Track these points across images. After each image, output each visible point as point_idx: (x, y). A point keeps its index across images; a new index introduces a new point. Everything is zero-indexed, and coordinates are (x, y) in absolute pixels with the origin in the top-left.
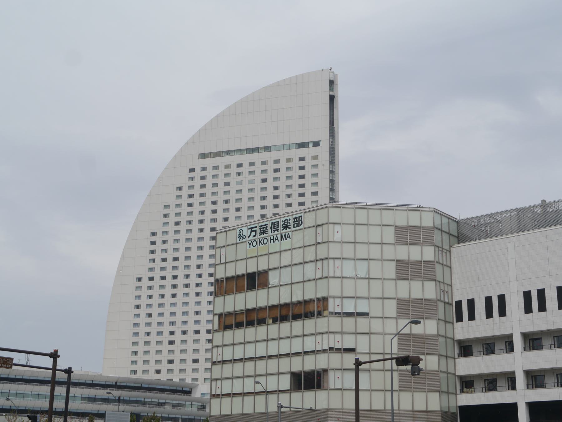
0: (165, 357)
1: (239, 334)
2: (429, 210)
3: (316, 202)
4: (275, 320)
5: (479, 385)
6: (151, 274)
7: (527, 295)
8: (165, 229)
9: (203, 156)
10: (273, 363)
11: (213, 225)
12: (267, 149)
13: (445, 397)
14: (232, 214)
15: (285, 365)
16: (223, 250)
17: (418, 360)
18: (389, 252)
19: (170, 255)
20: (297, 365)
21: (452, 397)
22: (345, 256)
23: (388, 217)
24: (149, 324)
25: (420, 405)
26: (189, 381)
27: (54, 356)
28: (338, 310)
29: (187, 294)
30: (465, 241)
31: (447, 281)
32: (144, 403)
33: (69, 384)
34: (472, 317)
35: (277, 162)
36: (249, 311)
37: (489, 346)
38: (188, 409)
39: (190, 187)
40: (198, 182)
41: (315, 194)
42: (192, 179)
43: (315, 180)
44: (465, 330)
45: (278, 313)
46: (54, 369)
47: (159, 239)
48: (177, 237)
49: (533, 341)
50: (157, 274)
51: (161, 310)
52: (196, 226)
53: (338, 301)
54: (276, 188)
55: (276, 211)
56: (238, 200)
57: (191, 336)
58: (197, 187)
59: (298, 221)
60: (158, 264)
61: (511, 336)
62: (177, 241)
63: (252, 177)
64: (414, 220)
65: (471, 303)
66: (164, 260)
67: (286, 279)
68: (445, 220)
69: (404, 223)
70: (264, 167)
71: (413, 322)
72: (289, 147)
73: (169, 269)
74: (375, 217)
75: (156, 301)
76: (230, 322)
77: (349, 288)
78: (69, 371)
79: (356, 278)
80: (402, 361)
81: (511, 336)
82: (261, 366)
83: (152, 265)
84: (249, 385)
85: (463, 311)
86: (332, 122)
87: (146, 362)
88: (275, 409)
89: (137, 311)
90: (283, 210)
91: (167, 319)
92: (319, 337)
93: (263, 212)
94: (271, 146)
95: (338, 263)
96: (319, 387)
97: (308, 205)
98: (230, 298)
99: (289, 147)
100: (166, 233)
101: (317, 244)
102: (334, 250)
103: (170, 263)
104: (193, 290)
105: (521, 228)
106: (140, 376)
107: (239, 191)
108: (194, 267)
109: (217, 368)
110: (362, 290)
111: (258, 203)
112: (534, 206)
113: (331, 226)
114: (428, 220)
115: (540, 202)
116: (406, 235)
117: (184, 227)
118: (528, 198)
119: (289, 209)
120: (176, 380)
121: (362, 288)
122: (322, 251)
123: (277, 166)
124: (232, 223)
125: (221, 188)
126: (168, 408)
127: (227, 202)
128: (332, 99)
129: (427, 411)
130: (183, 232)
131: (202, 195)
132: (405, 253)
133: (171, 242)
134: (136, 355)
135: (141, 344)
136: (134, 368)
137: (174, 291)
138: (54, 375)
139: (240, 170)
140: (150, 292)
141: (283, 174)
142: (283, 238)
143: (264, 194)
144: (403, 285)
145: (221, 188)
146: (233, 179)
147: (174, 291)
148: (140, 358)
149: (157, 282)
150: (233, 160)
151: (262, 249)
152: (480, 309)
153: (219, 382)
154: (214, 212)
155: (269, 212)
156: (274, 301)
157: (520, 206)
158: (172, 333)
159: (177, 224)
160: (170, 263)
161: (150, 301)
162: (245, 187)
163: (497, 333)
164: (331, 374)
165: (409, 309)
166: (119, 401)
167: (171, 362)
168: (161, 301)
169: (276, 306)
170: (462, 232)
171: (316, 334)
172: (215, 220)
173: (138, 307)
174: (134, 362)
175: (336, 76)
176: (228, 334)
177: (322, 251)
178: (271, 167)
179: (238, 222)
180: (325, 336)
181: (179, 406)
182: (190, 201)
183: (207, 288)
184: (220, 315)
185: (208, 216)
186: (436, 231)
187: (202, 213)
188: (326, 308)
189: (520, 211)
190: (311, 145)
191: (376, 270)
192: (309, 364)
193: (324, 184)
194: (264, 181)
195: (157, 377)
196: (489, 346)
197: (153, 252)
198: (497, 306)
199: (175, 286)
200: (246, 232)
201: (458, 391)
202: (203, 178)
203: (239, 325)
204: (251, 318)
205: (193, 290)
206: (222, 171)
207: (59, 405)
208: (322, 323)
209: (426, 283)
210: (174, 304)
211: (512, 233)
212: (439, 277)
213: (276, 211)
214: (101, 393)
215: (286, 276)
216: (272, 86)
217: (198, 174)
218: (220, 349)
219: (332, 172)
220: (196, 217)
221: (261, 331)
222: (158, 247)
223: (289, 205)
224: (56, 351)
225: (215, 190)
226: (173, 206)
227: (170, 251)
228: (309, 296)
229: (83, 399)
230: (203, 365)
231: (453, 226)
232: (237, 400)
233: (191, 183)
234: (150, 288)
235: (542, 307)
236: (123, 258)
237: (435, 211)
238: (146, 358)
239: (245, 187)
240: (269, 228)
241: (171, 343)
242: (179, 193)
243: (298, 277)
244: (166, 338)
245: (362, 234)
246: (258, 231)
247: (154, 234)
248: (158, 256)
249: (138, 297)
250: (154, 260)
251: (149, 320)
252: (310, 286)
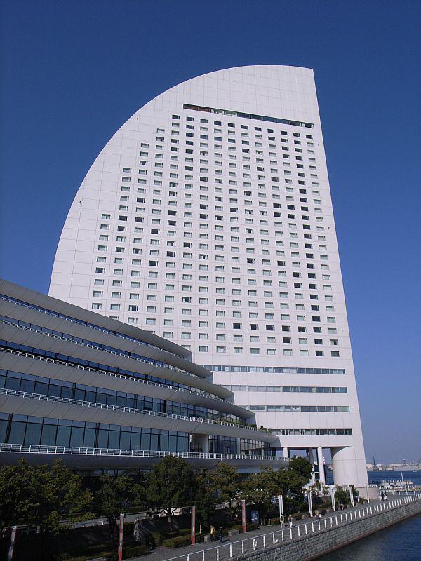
9: (186, 106)
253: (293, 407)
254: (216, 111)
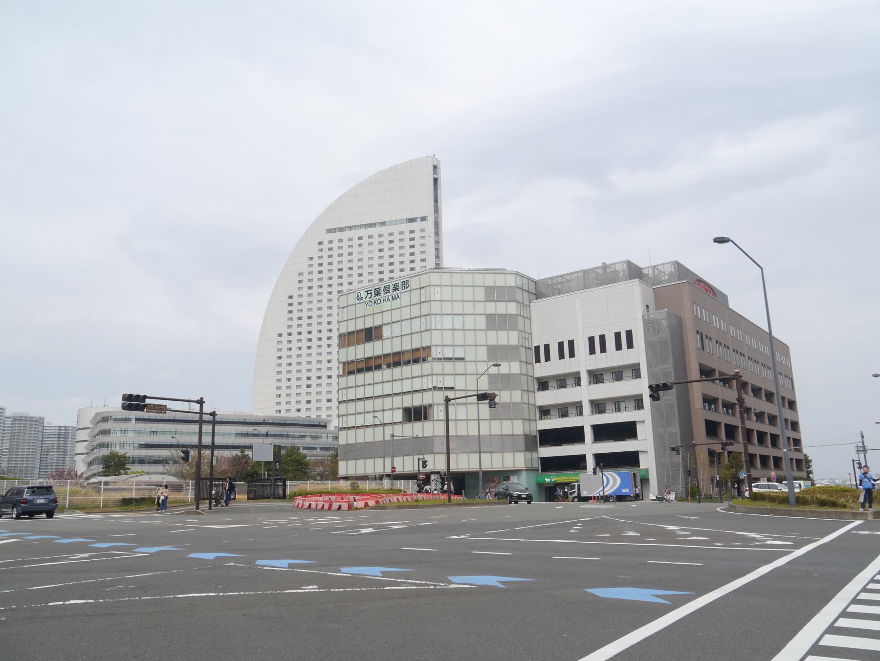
0: (304, 398)
1: (360, 378)
2: (512, 273)
3: (425, 267)
4: (389, 366)
5: (609, 407)
6: (290, 331)
7: (591, 340)
8: (300, 292)
9: (330, 231)
10: (388, 401)
11: (340, 288)
12: (383, 224)
13: (527, 423)
14: (355, 279)
15: (398, 402)
16: (345, 309)
17: (494, 395)
18: (480, 308)
19: (305, 315)
20: (409, 402)
21: (533, 423)
22: (455, 312)
23: (479, 279)
24: (289, 372)
25: (507, 431)
26: (324, 417)
27: (201, 402)
28: (440, 356)
29: (320, 346)
30: (542, 298)
31: (528, 330)
32: (288, 436)
33: (214, 423)
34: (548, 359)
35: (391, 234)
36: (368, 359)
37: (562, 381)
38: (324, 440)
39: (320, 257)
40: (326, 253)
41: (423, 260)
42: (321, 250)
43: (423, 249)
44: (543, 370)
45: (391, 360)
46: (201, 413)
47: (295, 301)
48: (310, 299)
49: (596, 377)
50: (295, 330)
51: (299, 360)
52: (326, 289)
53: (439, 349)
54: (391, 256)
55: (392, 275)
56: (360, 267)
57: (325, 380)
58: (325, 257)
59: (405, 284)
60: (296, 322)
61: (579, 373)
62: (310, 302)
63: (371, 248)
64: (500, 281)
65: (547, 347)
66: (300, 318)
67: (397, 332)
68: (525, 281)
69: (492, 284)
70: (381, 239)
71: (494, 365)
72: (401, 222)
73: (305, 325)
74: (468, 279)
75: (295, 352)
76: (352, 368)
77: (448, 339)
78: (213, 414)
79: (453, 330)
80: (482, 397)
81: (579, 373)
82: (378, 403)
83: (290, 323)
84: (369, 420)
85: (541, 354)
86: (436, 201)
87: (288, 403)
88: (389, 438)
89: (279, 361)
90: (397, 274)
91: (304, 367)
92: (424, 379)
93: (381, 276)
95: (439, 318)
96: (426, 418)
97: (418, 269)
98: (351, 349)
99: (401, 222)
100: (301, 296)
101: (421, 303)
102: (435, 308)
103: (305, 321)
104: (325, 342)
105: (586, 286)
106: (284, 414)
107: (360, 260)
108: (325, 324)
109: (343, 406)
110: (459, 340)
111: (376, 269)
112: (596, 268)
113: (432, 288)
114: (511, 281)
115: (601, 265)
116: (494, 294)
117: (316, 290)
118: (593, 262)
119: (402, 274)
120: (314, 416)
121: (459, 338)
122: (425, 309)
123: (391, 238)
124: (355, 286)
125: (346, 258)
126: (308, 440)
127: (351, 269)
128: (436, 181)
129: (513, 435)
130: (315, 294)
132: (491, 308)
133: (305, 303)
135: (284, 388)
136: (278, 408)
137: (309, 344)
138: (201, 417)
139: (360, 242)
140: (289, 346)
141: (396, 244)
142: (393, 299)
143: (381, 261)
144: (492, 334)
145: (346, 258)
146: (355, 250)
147: (309, 344)
148: (283, 399)
149: (295, 337)
151: (377, 308)
152: (554, 352)
153: (345, 418)
154: (340, 277)
155: (386, 276)
156: (387, 351)
157: (585, 268)
158: (309, 378)
159: (310, 288)
160: (305, 321)
161: (289, 353)
162: (365, 256)
163: (568, 371)
164: (435, 408)
165: (496, 353)
166: (267, 435)
167: (309, 402)
168: (299, 352)
169: (389, 355)
170: (539, 290)
171: (422, 376)
172: (341, 284)
173: (280, 358)
174: (278, 403)
175: (438, 161)
176: (351, 378)
177: (425, 309)
178: (386, 239)
179: (361, 285)
180: (430, 378)
181: (317, 437)
182: (320, 268)
183: (335, 341)
184: (344, 363)
185: (335, 281)
186: (518, 290)
187: (330, 278)
188: (429, 354)
189: (585, 272)
190: (419, 220)
191: (469, 323)
192: (417, 401)
193: (431, 252)
194: (381, 250)
195: (298, 414)
196: (562, 381)
197: (290, 312)
198: (568, 349)
199: (310, 340)
200: (363, 294)
201: (538, 418)
202: (330, 249)
203: (360, 371)
204: (370, 365)
205: (325, 342)
206: (345, 244)
207: (207, 440)
208: (426, 367)
209: (510, 332)
210: (309, 355)
211: (579, 290)
212: (521, 327)
213: (392, 275)
214: (250, 429)
215: (396, 329)
216: (386, 171)
217: (326, 246)
218: (345, 391)
219: (437, 242)
220: (325, 282)
221: (378, 374)
222: (295, 308)
223: (402, 270)
224: (202, 399)
225: (340, 259)
226: (306, 274)
227: (305, 311)
228: (416, 345)
229: (237, 434)
230: (334, 404)
231: (532, 285)
232: (360, 432)
233: (321, 254)
234: (290, 342)
235: (603, 349)
236: (266, 317)
237: (517, 274)
238: (288, 399)
239: (365, 256)
240: (382, 291)
241: (309, 386)
242: (311, 262)
243: (406, 330)
244: (304, 382)
245: (458, 294)
246: (373, 294)
247: (291, 297)
248: (295, 315)
249: (280, 350)
250: (291, 319)
251: (289, 368)
252: (406, 339)
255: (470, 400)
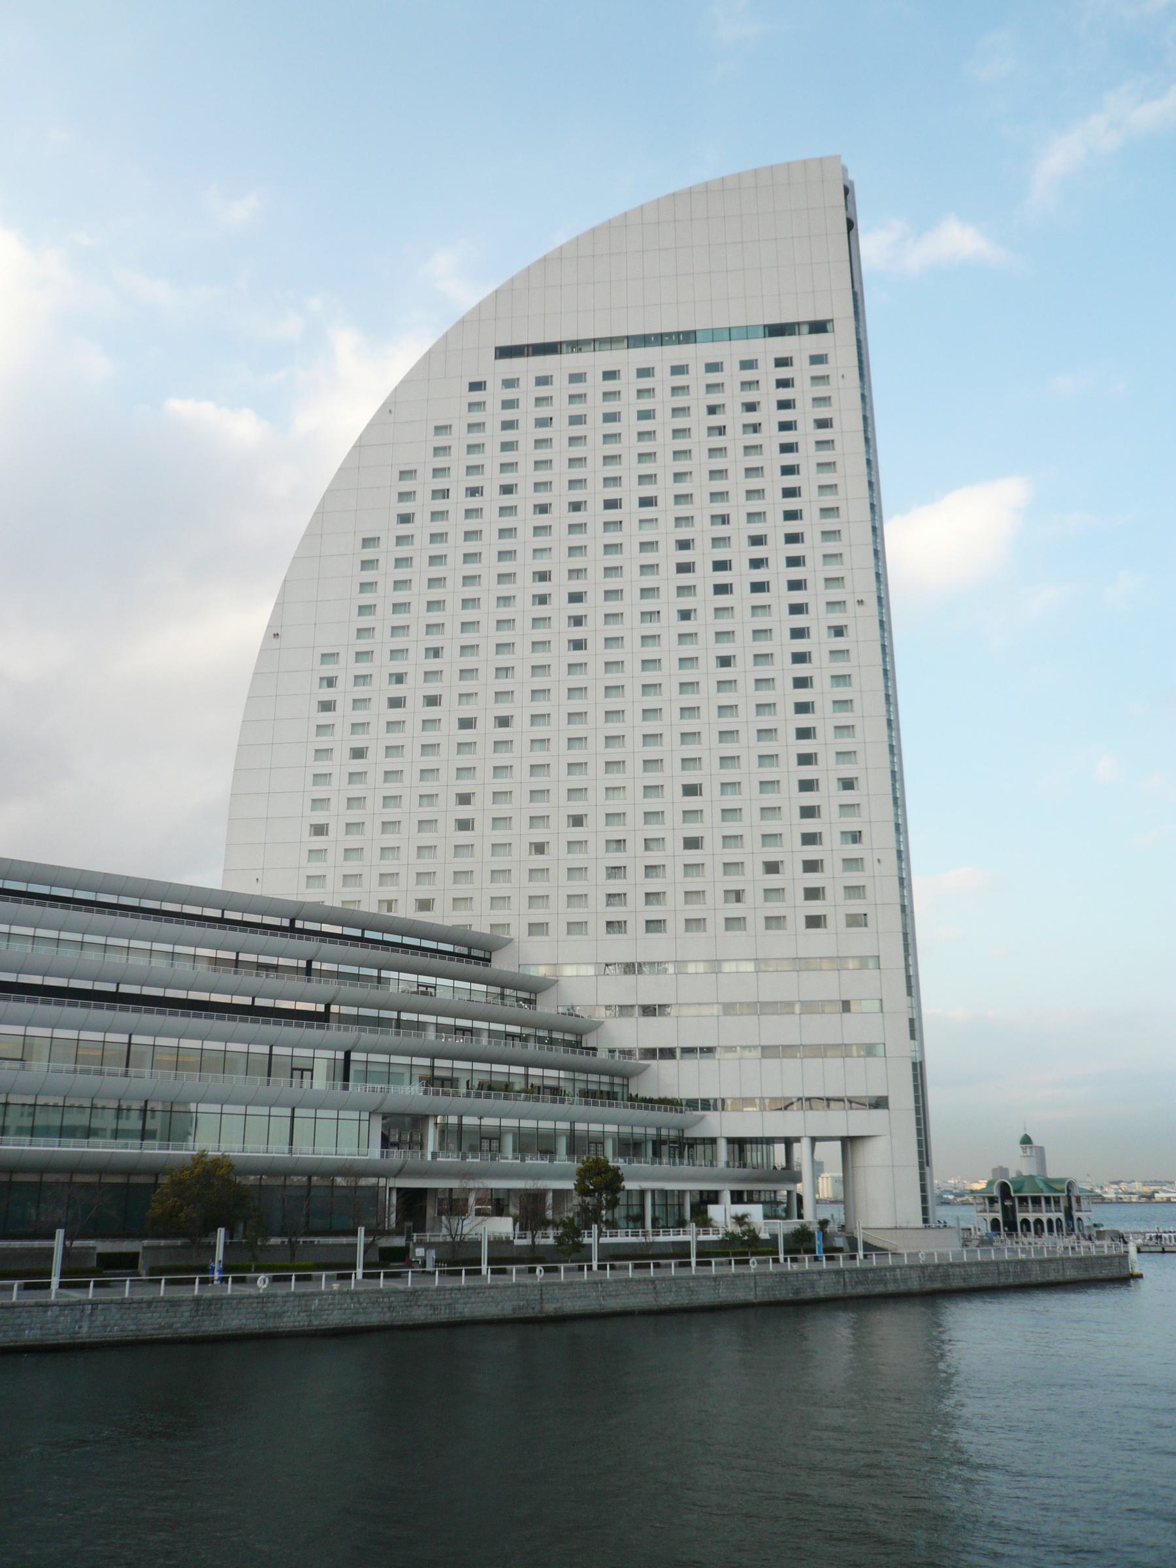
9: (505, 352)
72: (747, 332)
94: (695, 332)
99: (747, 332)
131: (361, 679)
134: (738, 900)
150: (593, 362)
175: (852, 183)
190: (805, 329)
197: (327, 706)
217: (494, 394)
253: (743, 1047)
254: (576, 345)
255: (705, 1011)
